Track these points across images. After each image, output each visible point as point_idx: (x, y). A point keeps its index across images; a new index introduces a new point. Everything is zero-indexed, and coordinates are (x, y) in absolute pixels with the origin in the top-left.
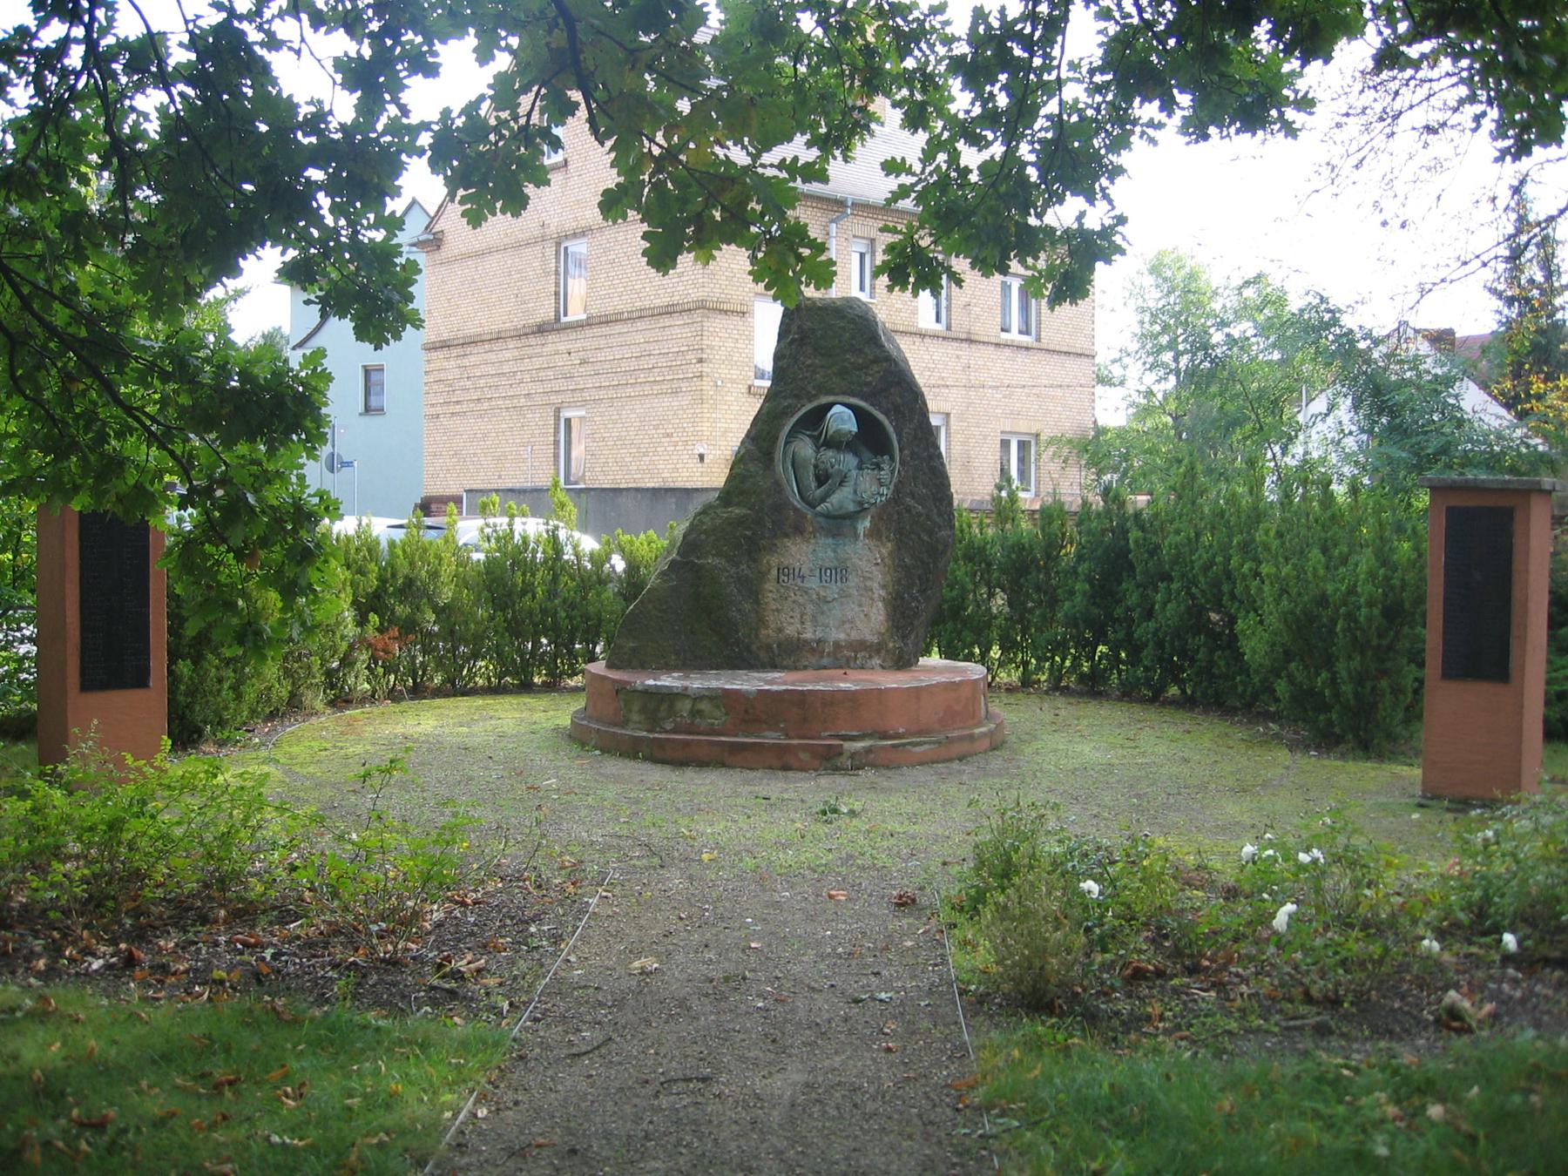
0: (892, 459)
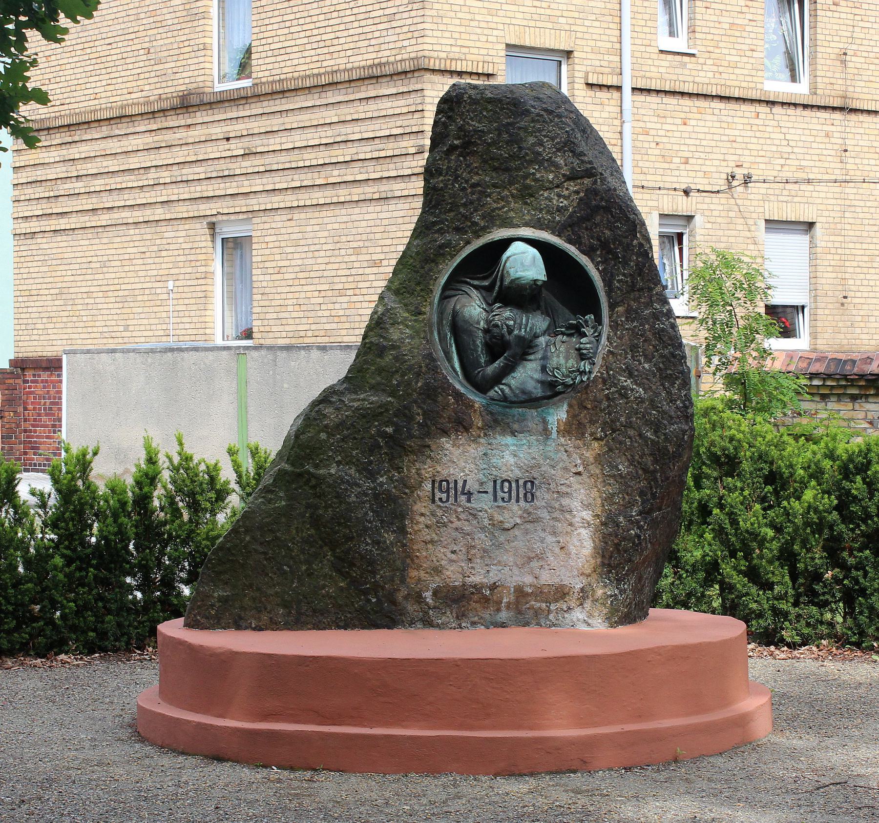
0: (599, 320)
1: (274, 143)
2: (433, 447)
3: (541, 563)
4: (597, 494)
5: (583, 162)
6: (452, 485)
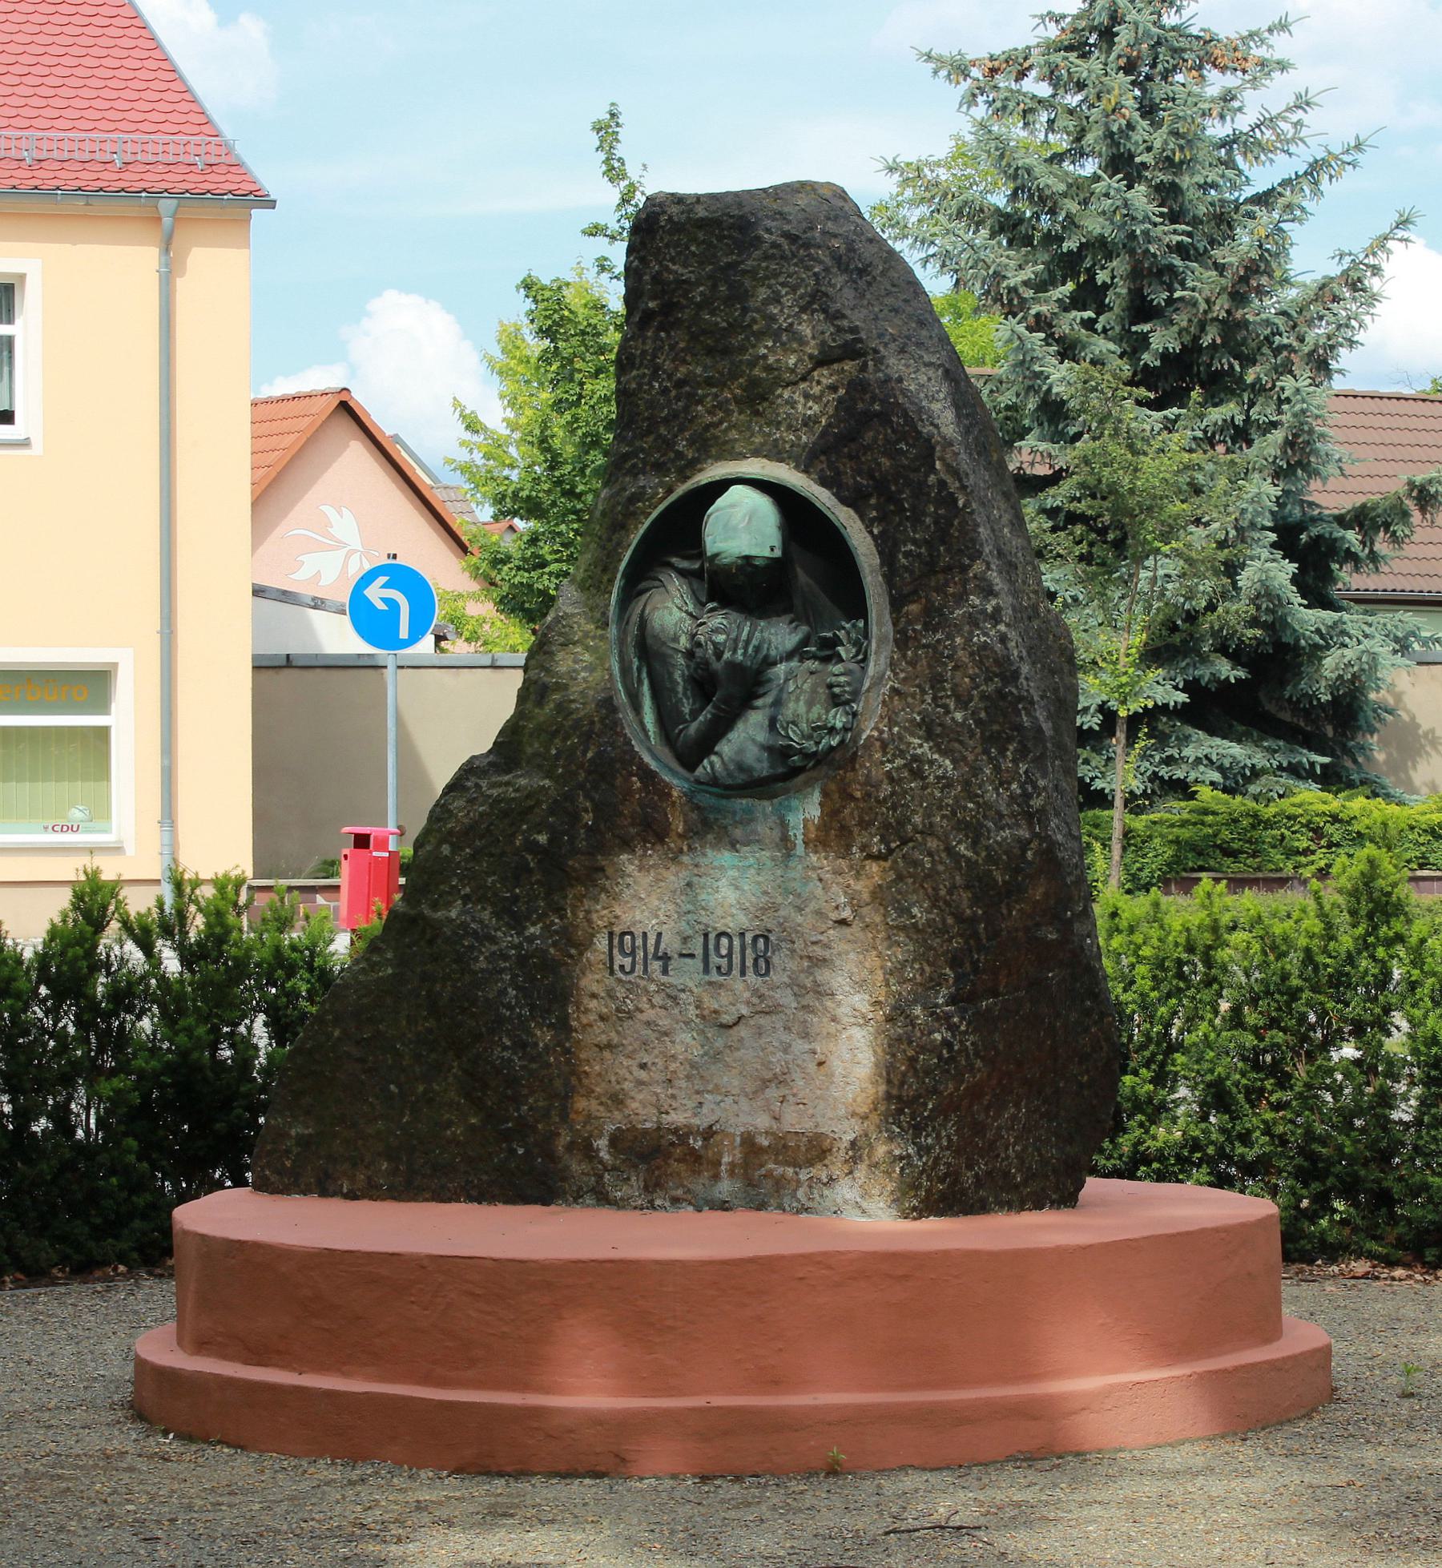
2: (609, 871)
3: (784, 1091)
4: (878, 962)
5: (839, 329)
6: (639, 942)
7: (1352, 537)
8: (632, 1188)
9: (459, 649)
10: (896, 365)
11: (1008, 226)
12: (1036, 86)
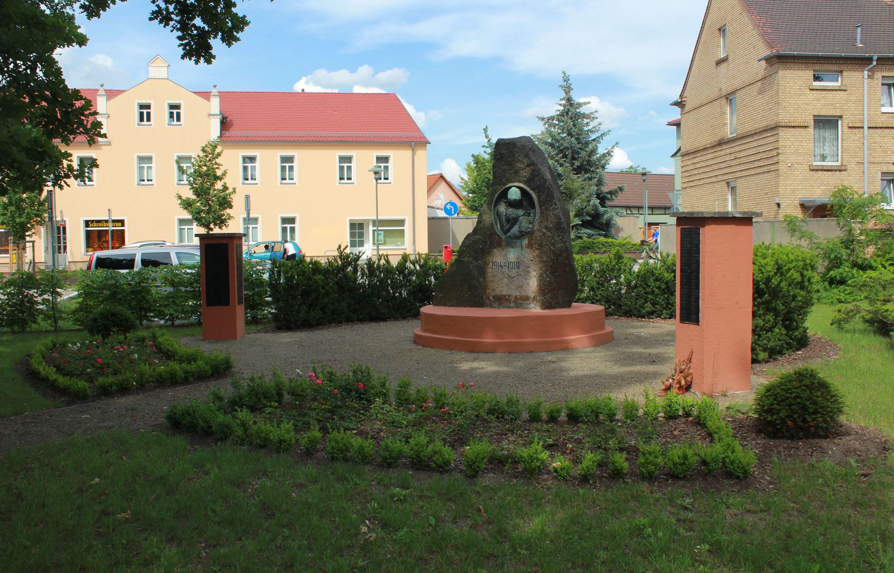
1: (742, 154)
7: (609, 196)
8: (496, 305)
9: (461, 216)
10: (540, 166)
11: (551, 145)
12: (556, 122)
